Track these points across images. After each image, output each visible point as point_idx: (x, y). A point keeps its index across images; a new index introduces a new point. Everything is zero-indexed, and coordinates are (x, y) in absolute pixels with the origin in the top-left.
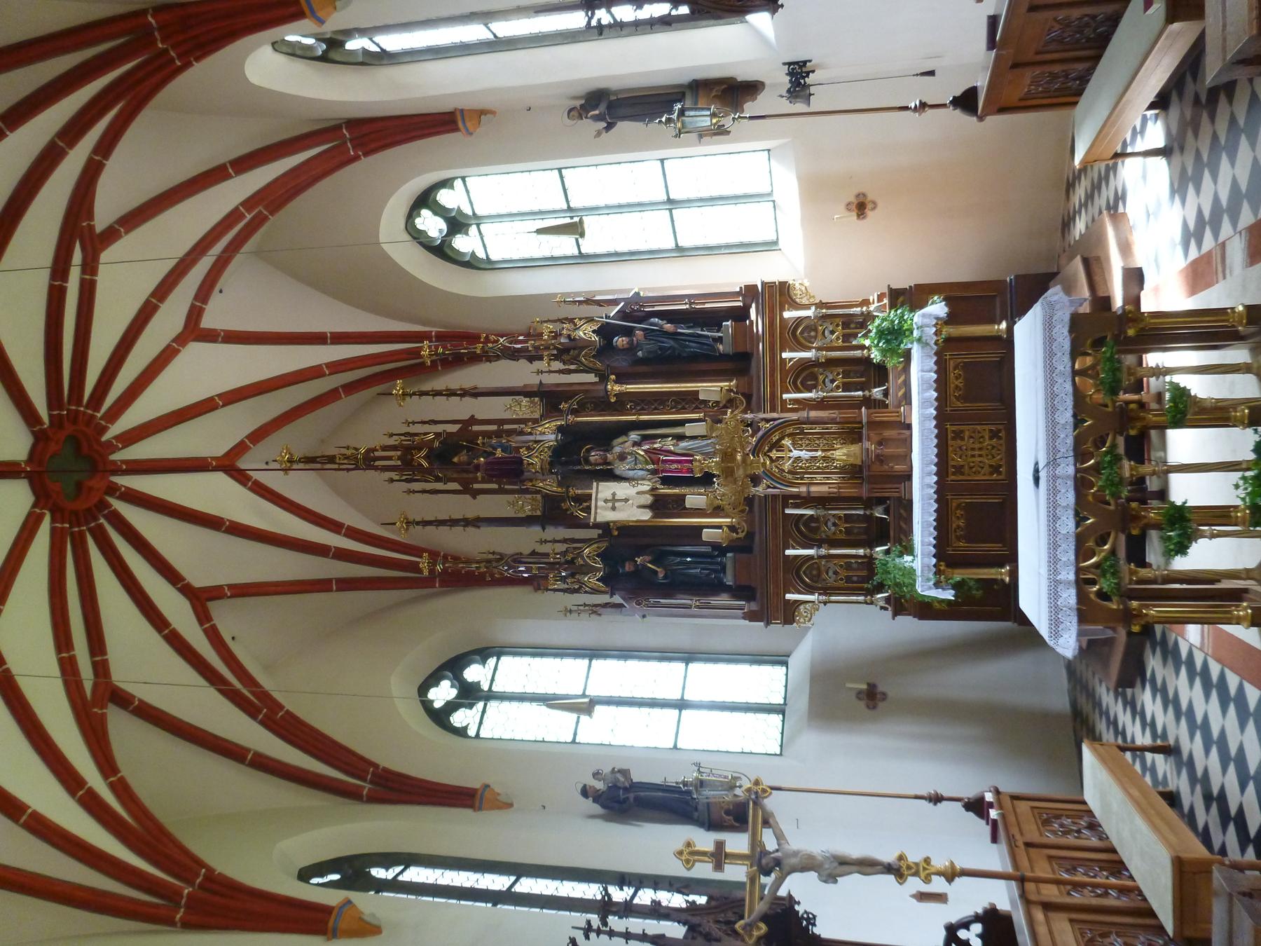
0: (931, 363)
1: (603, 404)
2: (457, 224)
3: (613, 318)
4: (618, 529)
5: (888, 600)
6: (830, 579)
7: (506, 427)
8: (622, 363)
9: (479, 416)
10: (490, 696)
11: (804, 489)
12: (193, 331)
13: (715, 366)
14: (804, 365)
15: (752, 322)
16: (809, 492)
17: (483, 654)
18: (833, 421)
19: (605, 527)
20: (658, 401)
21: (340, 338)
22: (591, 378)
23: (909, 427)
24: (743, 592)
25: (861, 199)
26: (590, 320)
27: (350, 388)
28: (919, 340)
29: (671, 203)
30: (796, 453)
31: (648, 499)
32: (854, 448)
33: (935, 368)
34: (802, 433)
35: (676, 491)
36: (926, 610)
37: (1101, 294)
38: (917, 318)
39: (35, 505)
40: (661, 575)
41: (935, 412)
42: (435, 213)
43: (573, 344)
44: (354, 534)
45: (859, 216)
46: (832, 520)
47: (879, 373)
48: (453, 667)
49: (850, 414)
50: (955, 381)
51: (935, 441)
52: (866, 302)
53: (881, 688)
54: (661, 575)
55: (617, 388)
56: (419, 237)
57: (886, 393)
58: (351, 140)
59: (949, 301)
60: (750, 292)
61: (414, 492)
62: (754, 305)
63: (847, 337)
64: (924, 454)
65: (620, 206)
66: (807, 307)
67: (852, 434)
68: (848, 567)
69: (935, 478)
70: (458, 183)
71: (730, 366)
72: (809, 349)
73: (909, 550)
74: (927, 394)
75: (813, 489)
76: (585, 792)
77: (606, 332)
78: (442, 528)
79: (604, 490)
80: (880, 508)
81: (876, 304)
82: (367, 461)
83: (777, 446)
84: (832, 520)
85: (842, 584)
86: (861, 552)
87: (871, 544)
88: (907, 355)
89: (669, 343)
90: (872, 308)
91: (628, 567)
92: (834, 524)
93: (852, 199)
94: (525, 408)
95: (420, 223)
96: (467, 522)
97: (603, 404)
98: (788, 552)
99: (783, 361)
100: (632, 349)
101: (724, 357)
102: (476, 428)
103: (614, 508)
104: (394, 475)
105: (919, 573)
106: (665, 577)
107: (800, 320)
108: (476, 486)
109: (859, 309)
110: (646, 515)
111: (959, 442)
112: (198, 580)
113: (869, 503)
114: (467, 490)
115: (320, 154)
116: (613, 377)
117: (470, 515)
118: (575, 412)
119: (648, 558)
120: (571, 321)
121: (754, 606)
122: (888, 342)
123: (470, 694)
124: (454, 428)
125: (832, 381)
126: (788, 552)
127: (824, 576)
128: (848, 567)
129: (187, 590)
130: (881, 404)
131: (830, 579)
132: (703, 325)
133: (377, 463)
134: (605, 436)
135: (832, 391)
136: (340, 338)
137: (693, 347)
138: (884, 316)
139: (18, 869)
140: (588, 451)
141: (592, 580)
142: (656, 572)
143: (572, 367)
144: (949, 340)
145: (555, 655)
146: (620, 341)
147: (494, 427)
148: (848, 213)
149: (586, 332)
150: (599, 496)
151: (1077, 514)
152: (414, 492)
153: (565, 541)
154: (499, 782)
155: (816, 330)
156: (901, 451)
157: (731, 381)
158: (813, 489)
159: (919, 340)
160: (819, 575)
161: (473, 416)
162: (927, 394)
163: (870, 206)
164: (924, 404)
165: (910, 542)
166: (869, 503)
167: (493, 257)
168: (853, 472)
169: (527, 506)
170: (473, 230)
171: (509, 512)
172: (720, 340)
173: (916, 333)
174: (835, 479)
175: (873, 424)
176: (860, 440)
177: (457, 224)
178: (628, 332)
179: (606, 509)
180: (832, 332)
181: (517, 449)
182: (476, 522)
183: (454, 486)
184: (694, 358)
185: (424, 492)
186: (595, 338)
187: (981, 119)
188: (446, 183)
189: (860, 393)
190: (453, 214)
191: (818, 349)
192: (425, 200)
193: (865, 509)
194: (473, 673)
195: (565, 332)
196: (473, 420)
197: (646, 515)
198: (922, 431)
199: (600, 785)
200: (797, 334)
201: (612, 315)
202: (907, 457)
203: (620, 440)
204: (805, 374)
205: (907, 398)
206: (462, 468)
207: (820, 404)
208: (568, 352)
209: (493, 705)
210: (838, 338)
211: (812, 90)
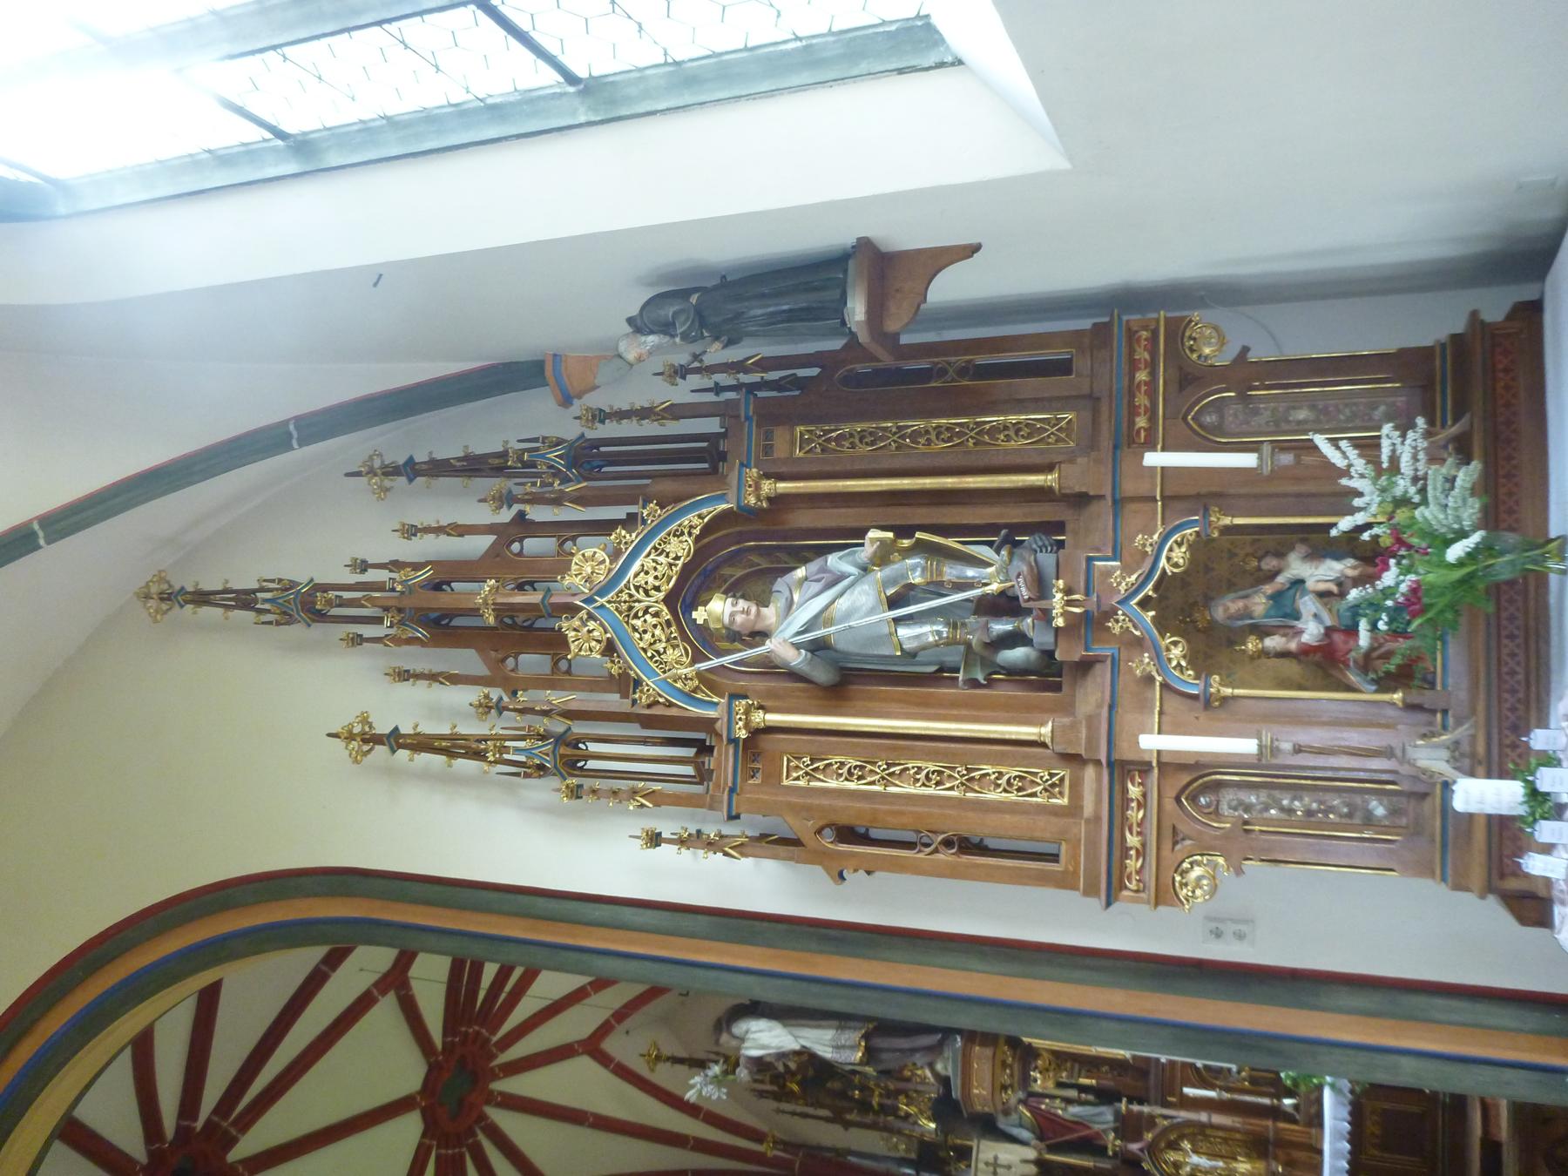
0: (1345, 1113)
12: (592, 1047)
23: (1320, 1152)
30: (1195, 1159)
33: (1349, 1118)
35: (1143, 594)
39: (424, 1135)
41: (1347, 1166)
50: (1372, 1128)
61: (784, 1112)
83: (1173, 1145)
139: (178, 895)
150: (981, 1156)
152: (784, 1112)
183: (825, 1113)
185: (794, 1114)
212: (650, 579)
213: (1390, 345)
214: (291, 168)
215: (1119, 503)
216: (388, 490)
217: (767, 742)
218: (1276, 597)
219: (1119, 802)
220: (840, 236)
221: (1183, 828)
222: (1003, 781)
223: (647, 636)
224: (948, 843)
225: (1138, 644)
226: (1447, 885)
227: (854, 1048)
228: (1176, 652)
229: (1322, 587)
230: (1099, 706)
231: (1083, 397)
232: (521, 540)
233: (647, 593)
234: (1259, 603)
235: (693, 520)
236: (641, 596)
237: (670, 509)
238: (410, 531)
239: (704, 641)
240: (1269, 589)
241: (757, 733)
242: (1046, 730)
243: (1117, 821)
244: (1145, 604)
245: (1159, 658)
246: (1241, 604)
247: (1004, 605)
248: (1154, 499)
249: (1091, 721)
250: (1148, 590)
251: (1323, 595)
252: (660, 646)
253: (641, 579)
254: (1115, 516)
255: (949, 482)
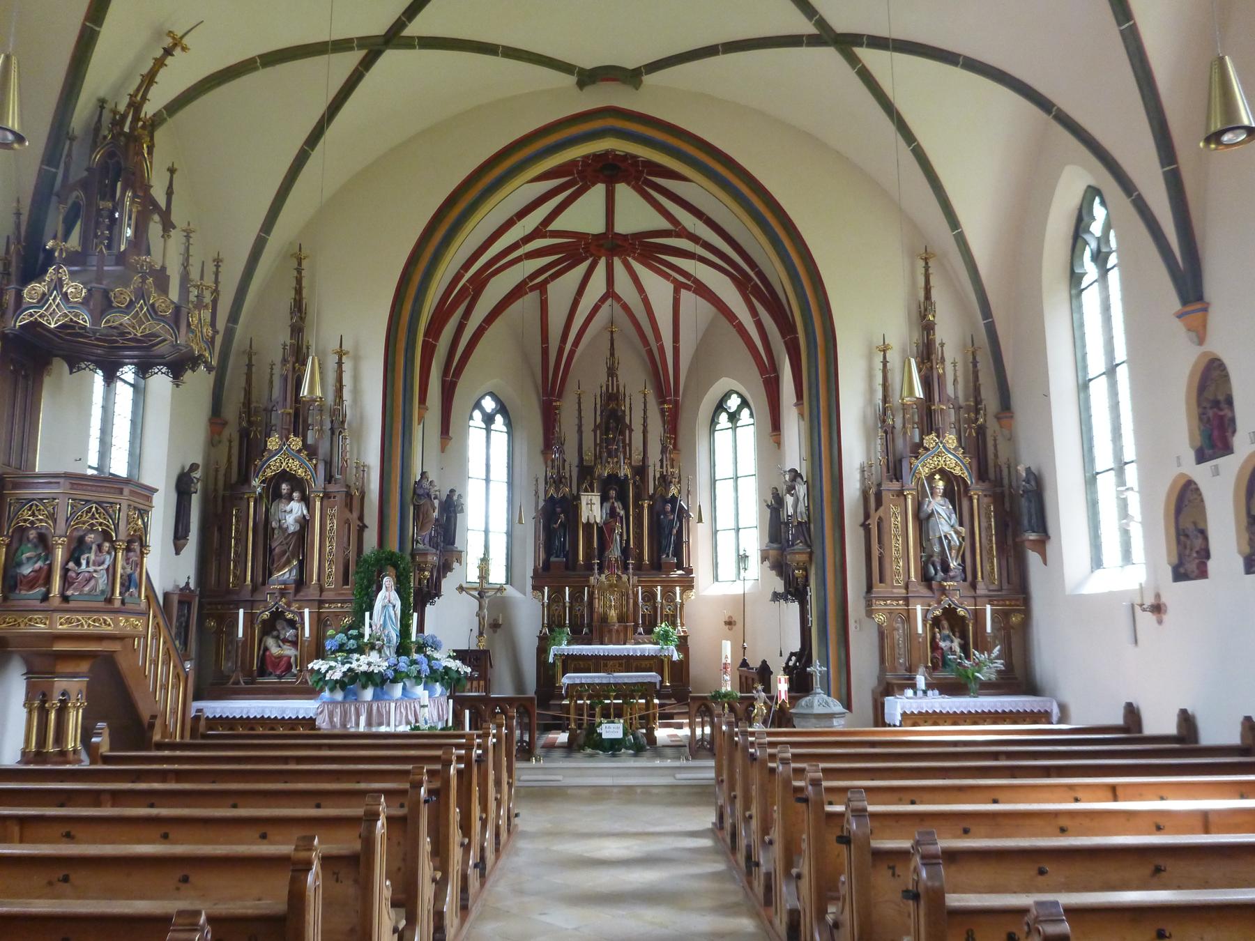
0: (652, 653)
1: (638, 497)
2: (733, 417)
3: (680, 503)
4: (577, 505)
5: (545, 634)
6: (554, 607)
7: (628, 448)
8: (658, 507)
9: (633, 434)
10: (488, 430)
11: (597, 596)
12: (610, 294)
13: (655, 555)
14: (655, 596)
15: (675, 571)
16: (595, 598)
17: (509, 423)
18: (628, 609)
19: (578, 498)
20: (639, 524)
21: (676, 351)
22: (651, 491)
23: (625, 644)
24: (547, 565)
25: (733, 623)
26: (679, 492)
27: (650, 352)
28: (662, 648)
29: (738, 530)
31: (592, 521)
32: (615, 619)
34: (623, 595)
36: (542, 651)
37: (675, 716)
38: (672, 647)
40: (555, 526)
42: (738, 406)
43: (667, 483)
44: (572, 353)
45: (725, 622)
46: (581, 609)
47: (649, 631)
48: (502, 409)
49: (631, 618)
51: (618, 655)
52: (682, 625)
53: (499, 630)
54: (555, 526)
55: (646, 505)
56: (727, 396)
57: (640, 634)
58: (770, 377)
59: (681, 662)
60: (689, 571)
62: (684, 573)
63: (667, 616)
64: (612, 649)
65: (737, 504)
66: (681, 598)
67: (622, 619)
68: (559, 616)
69: (602, 655)
70: (751, 421)
71: (655, 560)
72: (662, 598)
73: (569, 644)
74: (638, 651)
75: (597, 600)
76: (452, 491)
77: (674, 500)
78: (577, 412)
79: (596, 498)
80: (587, 631)
81: (681, 630)
82: (612, 372)
84: (581, 609)
85: (551, 612)
86: (567, 622)
87: (571, 626)
88: (657, 643)
89: (667, 532)
90: (679, 628)
91: (558, 510)
92: (579, 610)
93: (734, 619)
94: (637, 457)
95: (734, 396)
96: (580, 426)
97: (638, 497)
98: (567, 588)
99: (656, 586)
100: (665, 513)
101: (659, 558)
102: (627, 432)
103: (587, 504)
104: (604, 389)
105: (561, 647)
106: (554, 528)
107: (675, 594)
108: (598, 432)
109: (679, 622)
110: (584, 520)
111: (617, 665)
112: (550, 287)
113: (590, 625)
114: (596, 427)
115: (765, 363)
116: (651, 503)
117: (584, 428)
118: (634, 483)
119: (563, 520)
120: (679, 482)
121: (540, 571)
122: (663, 635)
123: (489, 419)
124: (627, 421)
125: (647, 609)
126: (567, 588)
127: (555, 605)
128: (559, 616)
129: (546, 282)
130: (635, 631)
131: (554, 607)
132: (675, 547)
133: (610, 378)
134: (623, 498)
135: (642, 609)
136: (676, 351)
137: (664, 543)
138: (675, 633)
140: (615, 490)
141: (552, 491)
142: (556, 524)
143: (657, 483)
144: (662, 661)
145: (508, 463)
146: (669, 507)
147: (627, 442)
148: (727, 617)
149: (673, 490)
151: (600, 684)
153: (571, 476)
154: (452, 445)
155: (671, 602)
156: (614, 639)
157: (648, 561)
158: (597, 600)
159: (662, 648)
160: (556, 602)
161: (633, 430)
162: (638, 651)
163: (730, 627)
164: (635, 650)
165: (573, 644)
166: (590, 625)
167: (716, 433)
168: (604, 619)
169: (589, 457)
170: (730, 425)
171: (585, 448)
172: (668, 556)
173: (665, 647)
174: (601, 610)
175: (626, 628)
176: (619, 622)
177: (733, 417)
178: (673, 510)
179: (587, 500)
180: (669, 609)
181: (617, 457)
182: (580, 431)
184: (660, 543)
186: (670, 495)
187: (738, 669)
188: (752, 415)
189: (641, 622)
190: (737, 417)
191: (662, 603)
192: (744, 403)
193: (587, 624)
194: (499, 419)
195: (674, 480)
196: (631, 431)
197: (584, 520)
198: (623, 649)
199: (455, 498)
200: (668, 594)
201: (682, 502)
202: (611, 643)
203: (621, 506)
204: (650, 596)
205: (638, 643)
206: (608, 423)
207: (636, 603)
208: (664, 481)
209: (484, 431)
210: (667, 612)
211: (778, 603)
212: (948, 463)
213: (1014, 661)
214: (1080, 382)
215: (974, 597)
216: (1170, 934)
217: (902, 498)
218: (949, 636)
219: (897, 599)
220: (1051, 531)
221: (893, 615)
222: (898, 568)
223: (931, 462)
224: (881, 553)
225: (939, 602)
226: (19, 762)
227: (802, 519)
228: (938, 613)
229: (953, 647)
230: (922, 593)
231: (1001, 587)
232: (953, 408)
233: (944, 461)
234: (946, 632)
235: (966, 475)
236: (943, 459)
237: (968, 466)
238: (954, 364)
239: (930, 478)
240: (951, 634)
241: (905, 497)
242: (913, 579)
243: (893, 599)
244: (950, 605)
245: (935, 609)
246: (946, 627)
247: (946, 568)
248: (976, 606)
249: (917, 591)
250: (953, 606)
251: (951, 648)
252: (928, 465)
253: (948, 459)
254: (970, 597)
255: (978, 551)
